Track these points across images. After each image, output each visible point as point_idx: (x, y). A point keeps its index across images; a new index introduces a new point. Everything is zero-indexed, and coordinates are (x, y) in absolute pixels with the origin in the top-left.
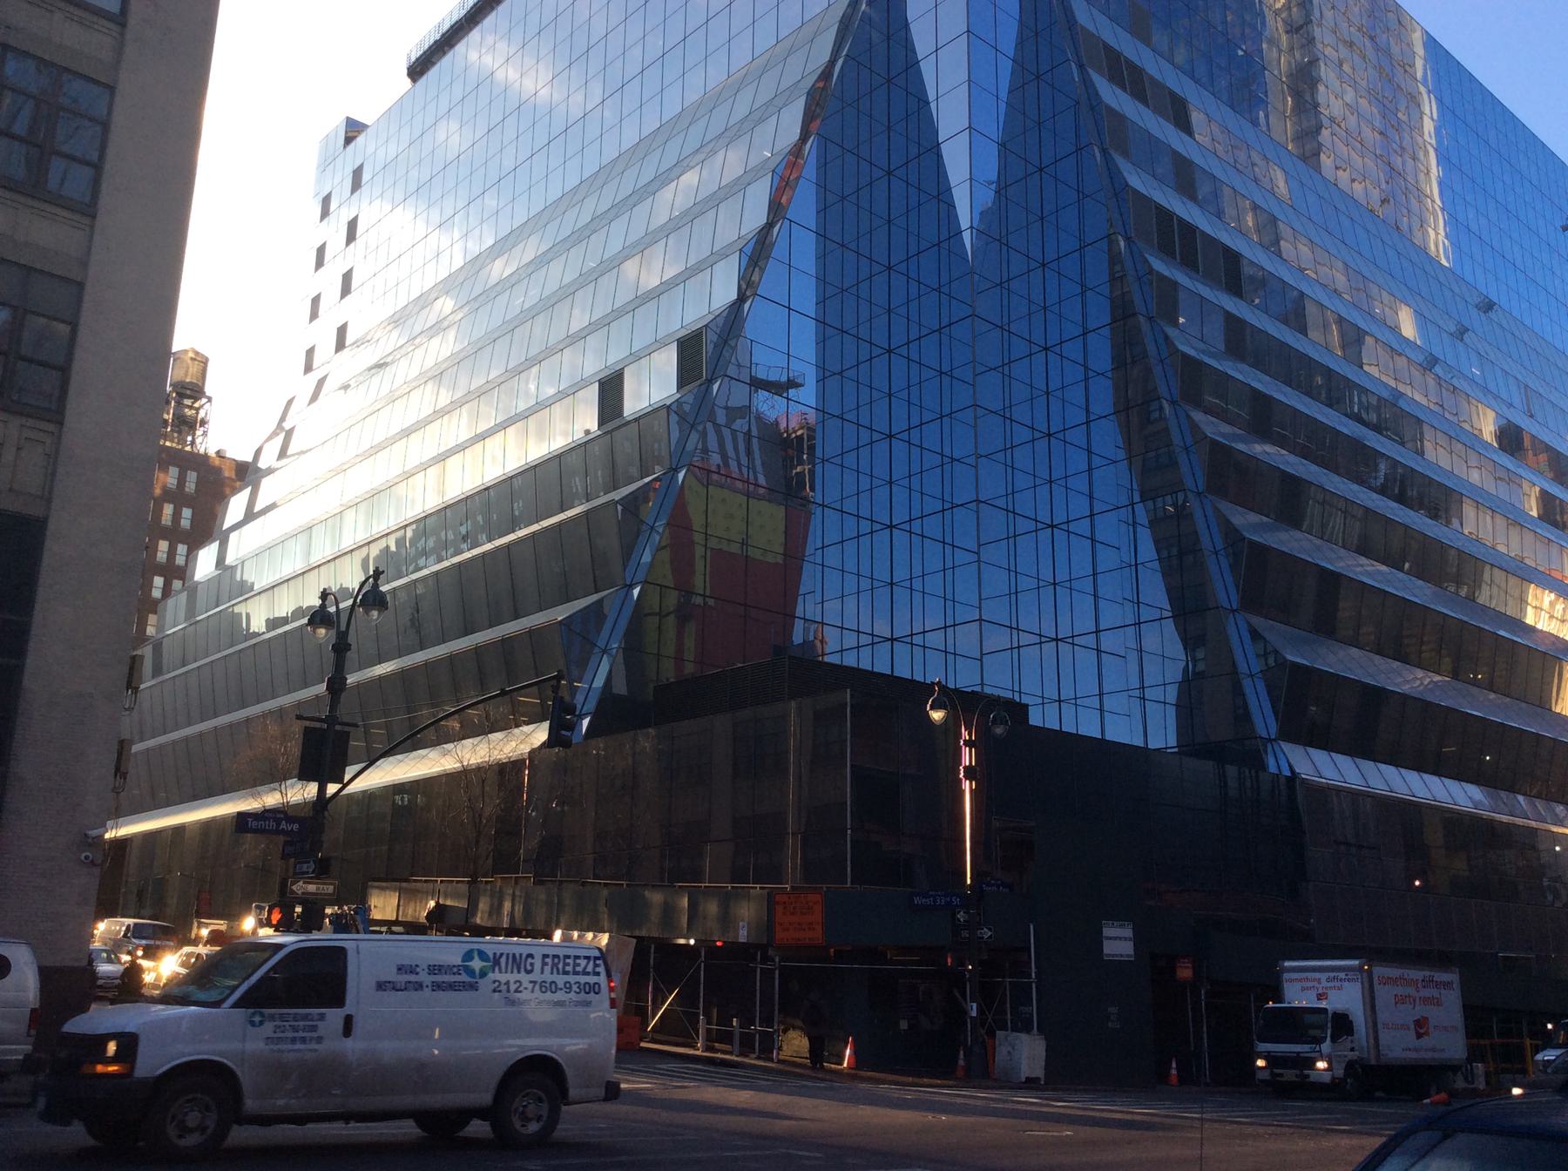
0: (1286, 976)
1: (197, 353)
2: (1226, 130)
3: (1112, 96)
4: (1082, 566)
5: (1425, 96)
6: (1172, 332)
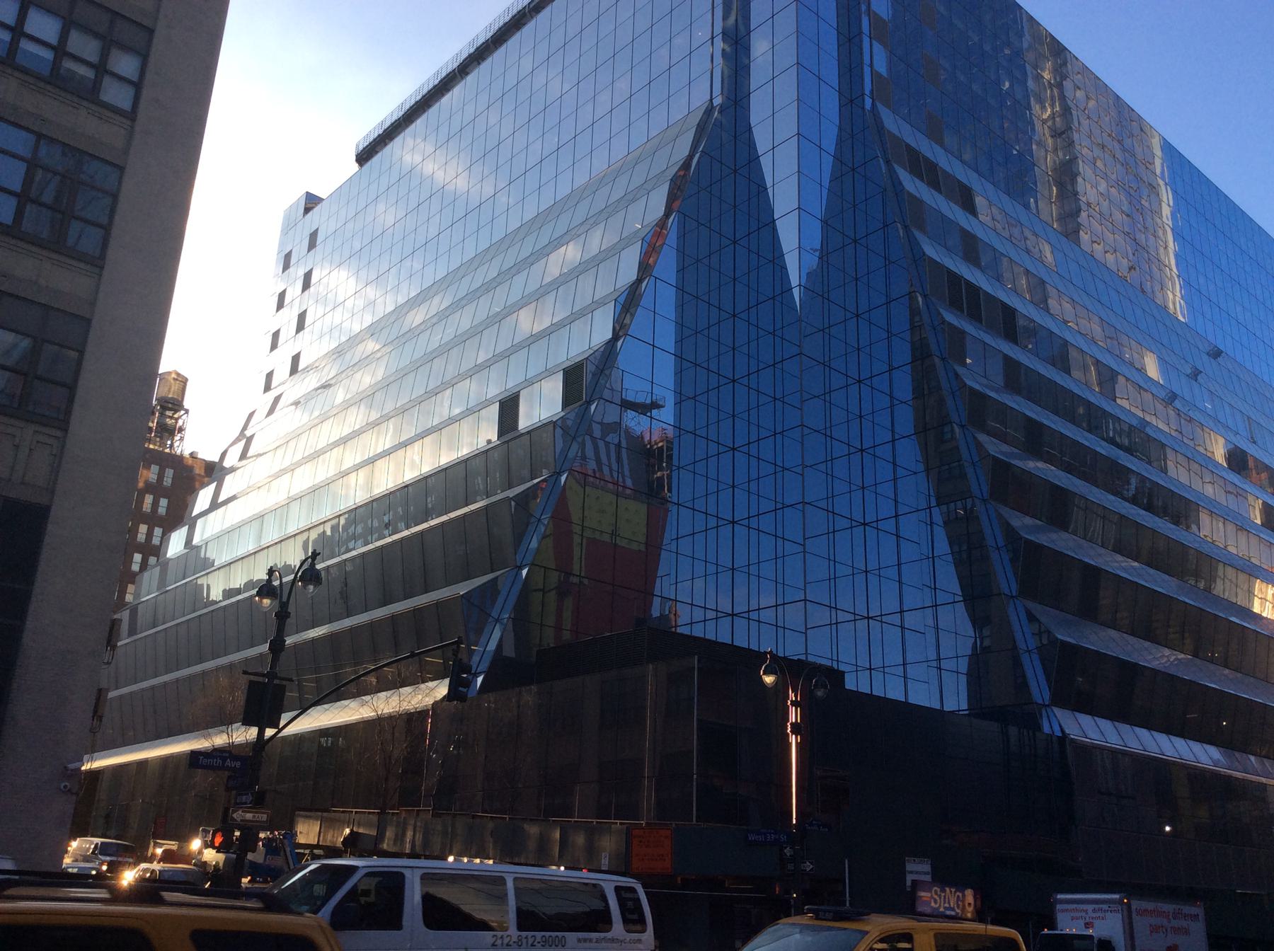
0: (1059, 907)
1: (178, 374)
3: (912, 184)
5: (1163, 187)
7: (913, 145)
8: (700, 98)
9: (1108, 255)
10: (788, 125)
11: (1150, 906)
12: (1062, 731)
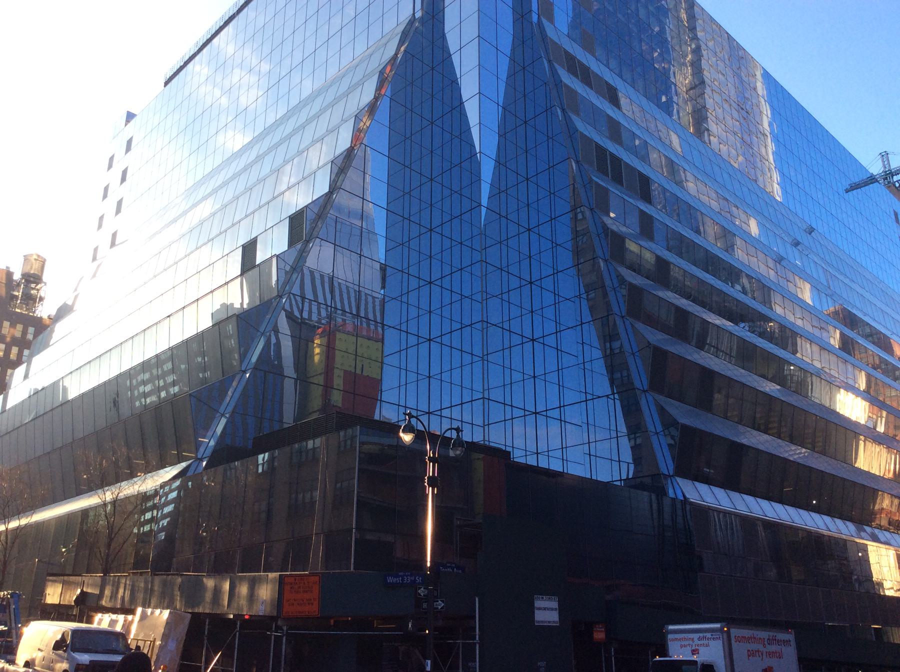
0: (670, 636)
1: (39, 256)
2: (641, 106)
3: (566, 78)
4: (552, 366)
5: (763, 103)
6: (605, 219)
7: (571, 51)
8: (406, 14)
9: (721, 146)
10: (471, 29)
11: (746, 633)
12: (684, 496)
